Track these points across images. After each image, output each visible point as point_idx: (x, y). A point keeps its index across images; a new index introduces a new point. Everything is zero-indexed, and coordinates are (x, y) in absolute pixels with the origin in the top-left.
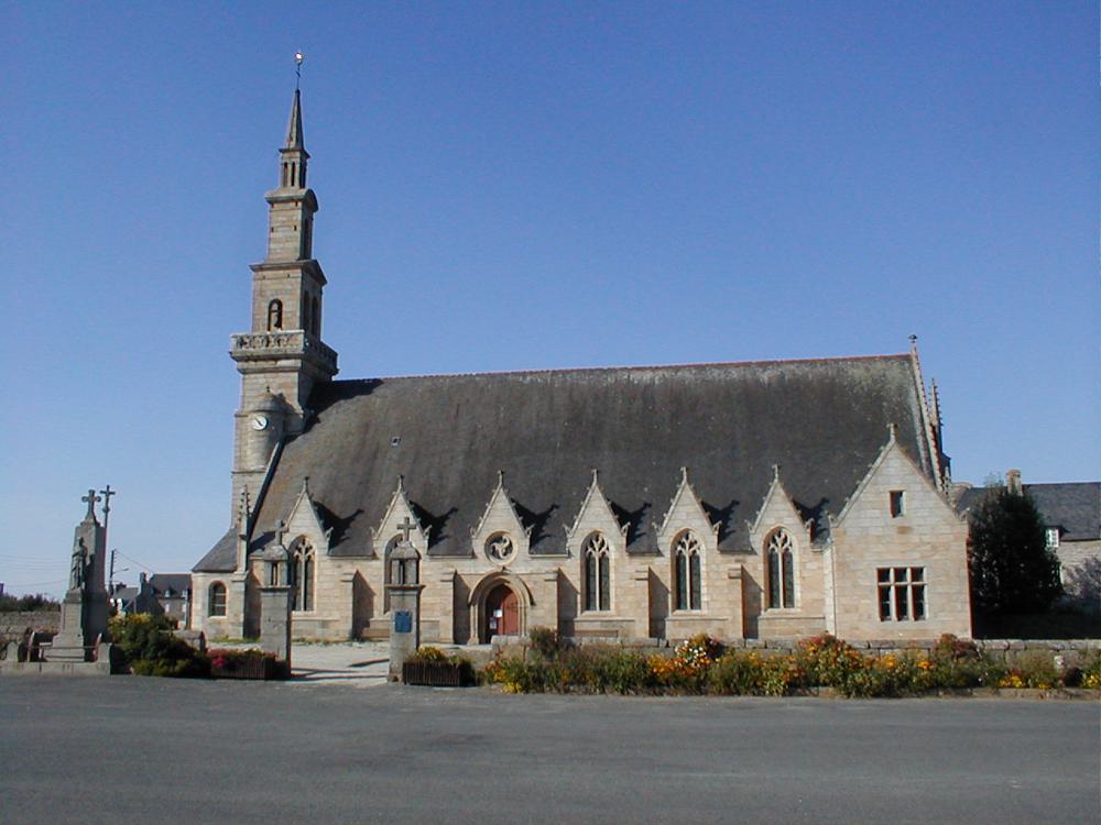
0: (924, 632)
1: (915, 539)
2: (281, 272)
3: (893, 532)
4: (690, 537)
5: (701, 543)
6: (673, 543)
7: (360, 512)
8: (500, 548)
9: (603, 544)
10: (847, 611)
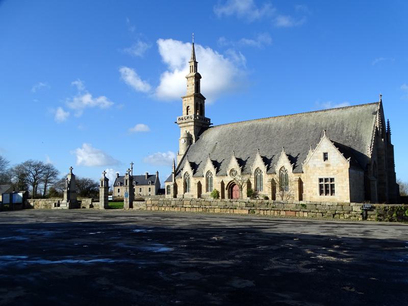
0: (334, 199)
1: (331, 168)
3: (324, 166)
8: (234, 173)
10: (309, 192)
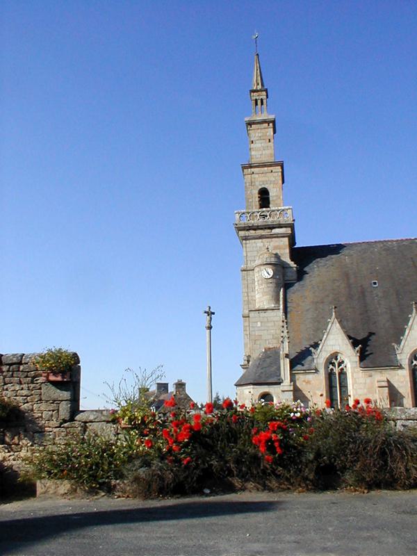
2: (266, 168)
4: (339, 358)
5: (347, 362)
6: (326, 363)
7: (371, 334)
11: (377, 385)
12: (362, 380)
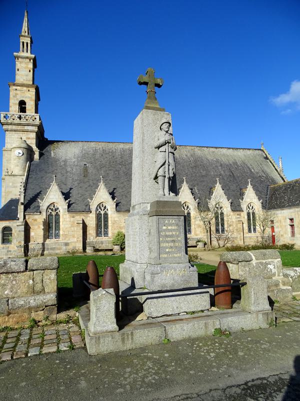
9: (188, 207)
11: (76, 222)
12: (68, 220)
